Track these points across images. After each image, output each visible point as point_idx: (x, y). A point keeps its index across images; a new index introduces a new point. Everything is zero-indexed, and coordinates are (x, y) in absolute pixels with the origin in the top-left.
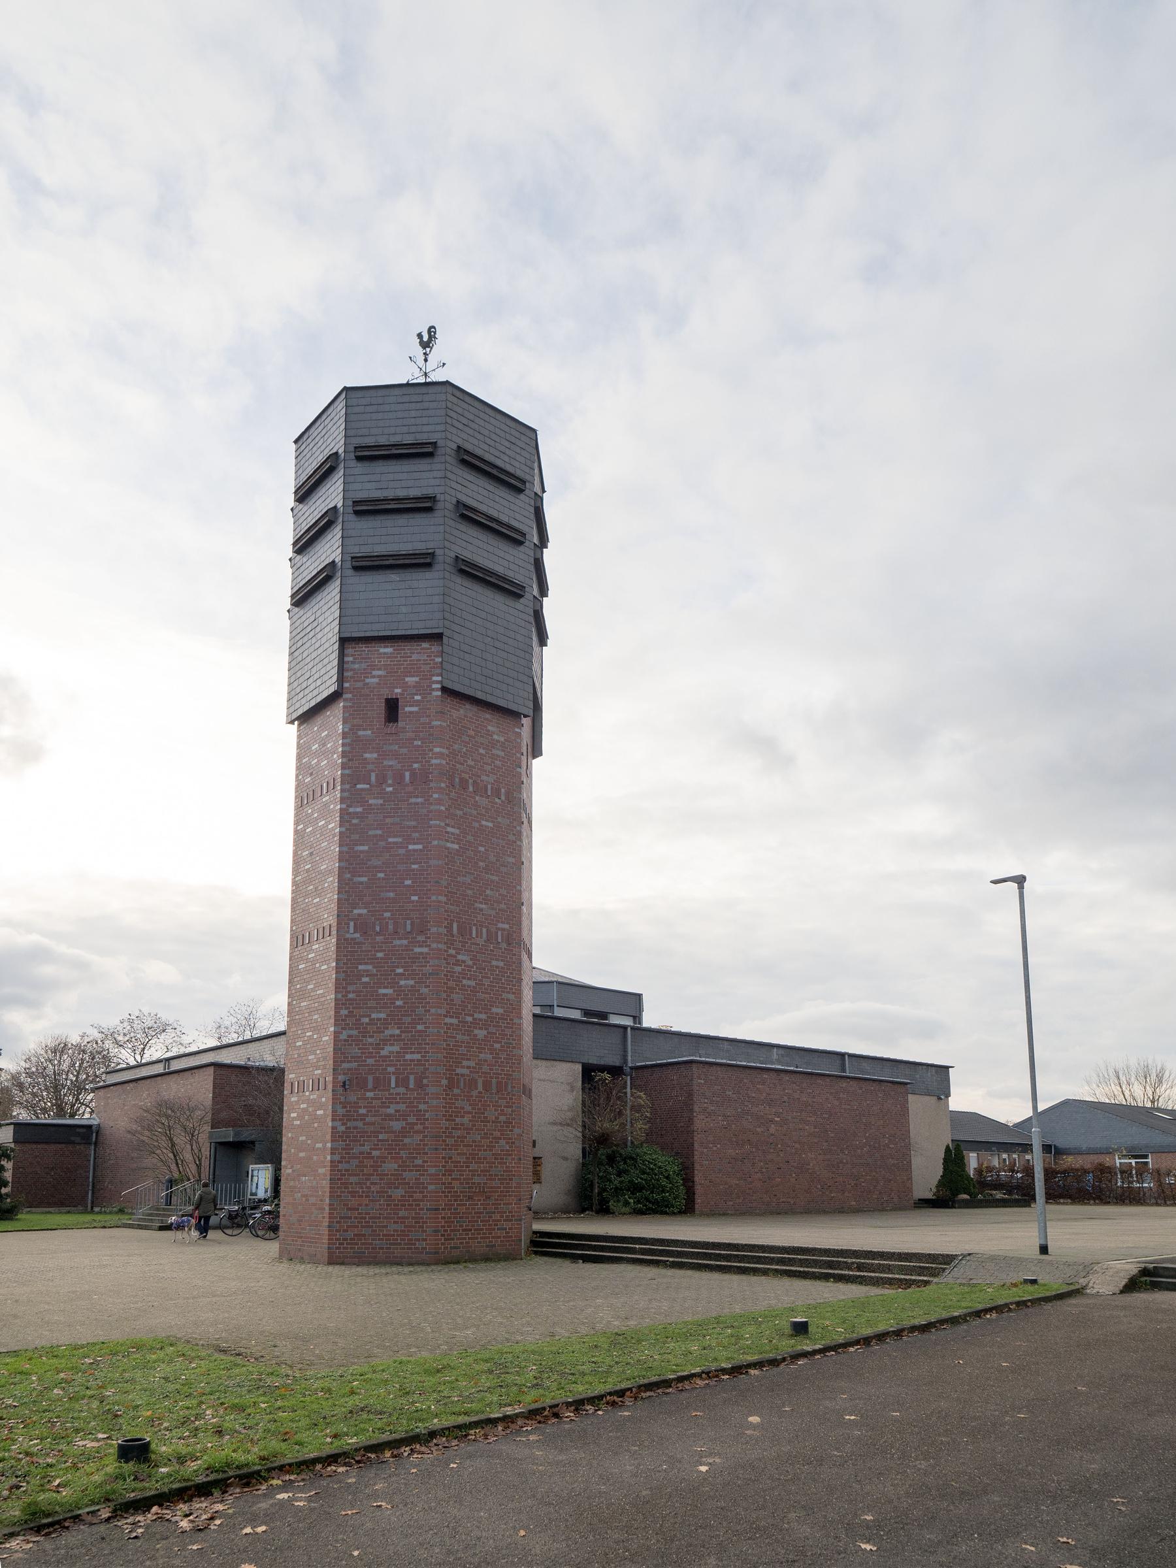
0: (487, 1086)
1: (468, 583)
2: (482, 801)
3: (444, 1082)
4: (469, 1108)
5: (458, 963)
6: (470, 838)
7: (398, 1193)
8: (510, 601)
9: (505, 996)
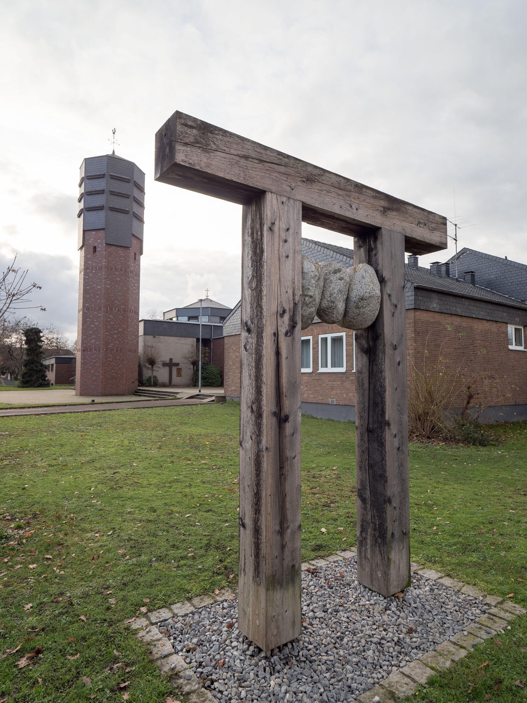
0: (117, 350)
1: (113, 212)
2: (117, 273)
3: (105, 349)
4: (111, 356)
5: (109, 318)
6: (113, 284)
7: (94, 378)
8: (126, 215)
9: (123, 326)
